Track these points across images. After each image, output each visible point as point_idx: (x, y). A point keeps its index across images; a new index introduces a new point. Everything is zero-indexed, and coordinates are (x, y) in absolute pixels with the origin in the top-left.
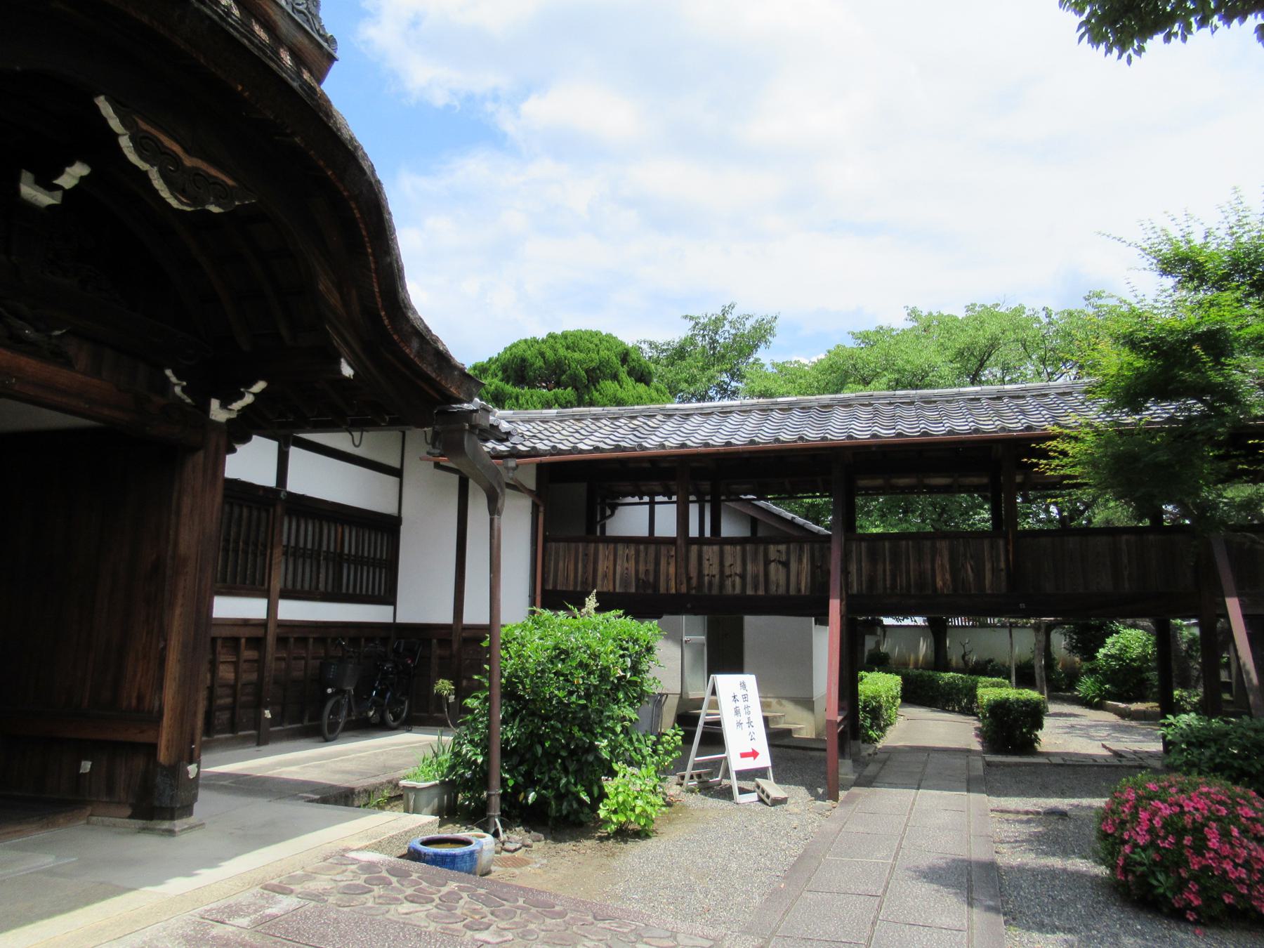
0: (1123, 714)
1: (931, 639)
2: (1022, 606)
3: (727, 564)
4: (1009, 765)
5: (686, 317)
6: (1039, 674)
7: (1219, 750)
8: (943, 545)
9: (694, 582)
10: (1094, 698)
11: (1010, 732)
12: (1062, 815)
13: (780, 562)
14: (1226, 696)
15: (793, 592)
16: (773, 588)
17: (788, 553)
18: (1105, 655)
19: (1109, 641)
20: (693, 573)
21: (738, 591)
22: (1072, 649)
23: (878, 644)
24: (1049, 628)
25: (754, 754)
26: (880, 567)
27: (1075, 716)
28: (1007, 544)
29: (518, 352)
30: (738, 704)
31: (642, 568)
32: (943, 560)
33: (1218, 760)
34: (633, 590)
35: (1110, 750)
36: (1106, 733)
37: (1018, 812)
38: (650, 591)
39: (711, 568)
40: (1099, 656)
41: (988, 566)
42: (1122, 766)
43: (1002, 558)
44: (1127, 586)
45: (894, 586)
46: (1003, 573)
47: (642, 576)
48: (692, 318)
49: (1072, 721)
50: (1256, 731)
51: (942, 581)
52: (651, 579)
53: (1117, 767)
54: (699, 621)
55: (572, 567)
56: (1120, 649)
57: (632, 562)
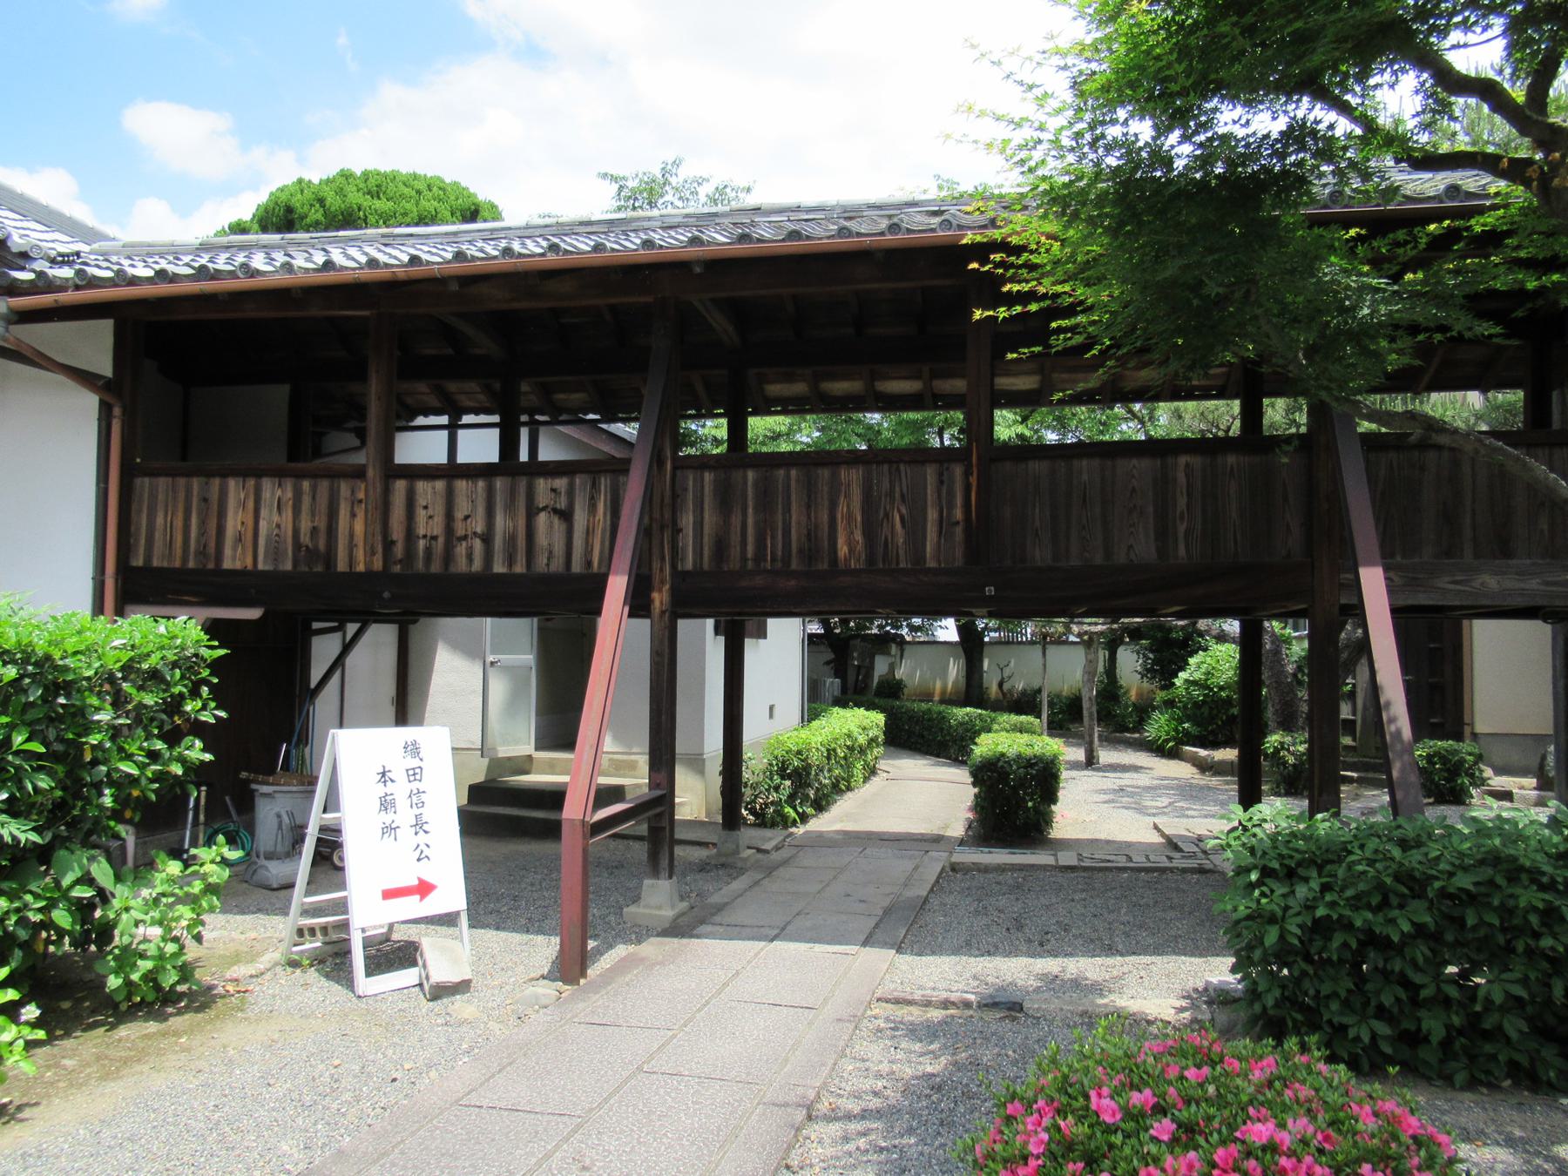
0: (1204, 767)
1: (962, 661)
2: (990, 590)
3: (459, 515)
4: (985, 869)
5: (605, 176)
6: (1089, 709)
7: (1325, 888)
8: (853, 477)
9: (399, 550)
10: (1167, 741)
11: (1014, 805)
12: (1006, 1006)
13: (555, 511)
14: (1347, 741)
15: (577, 567)
16: (541, 563)
17: (571, 493)
18: (1186, 681)
19: (1192, 661)
20: (397, 533)
21: (477, 565)
22: (1148, 672)
23: (892, 668)
24: (1113, 644)
25: (424, 889)
26: (736, 520)
27: (1136, 769)
28: (967, 473)
29: (284, 197)
30: (390, 787)
31: (305, 525)
32: (851, 505)
33: (1321, 912)
34: (288, 566)
35: (1163, 835)
36: (1165, 801)
37: (928, 1004)
38: (319, 568)
39: (429, 524)
40: (1178, 682)
41: (932, 515)
42: (1171, 870)
43: (959, 501)
44: (1182, 551)
45: (760, 556)
46: (959, 530)
47: (305, 539)
48: (614, 179)
49: (1128, 779)
50: (1404, 844)
51: (847, 544)
52: (322, 545)
53: (1163, 870)
54: (522, 629)
55: (179, 523)
56: (1208, 673)
57: (288, 513)
